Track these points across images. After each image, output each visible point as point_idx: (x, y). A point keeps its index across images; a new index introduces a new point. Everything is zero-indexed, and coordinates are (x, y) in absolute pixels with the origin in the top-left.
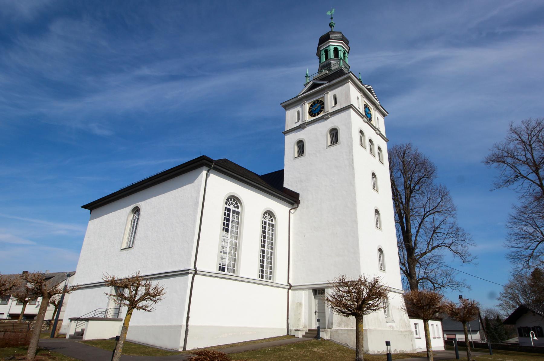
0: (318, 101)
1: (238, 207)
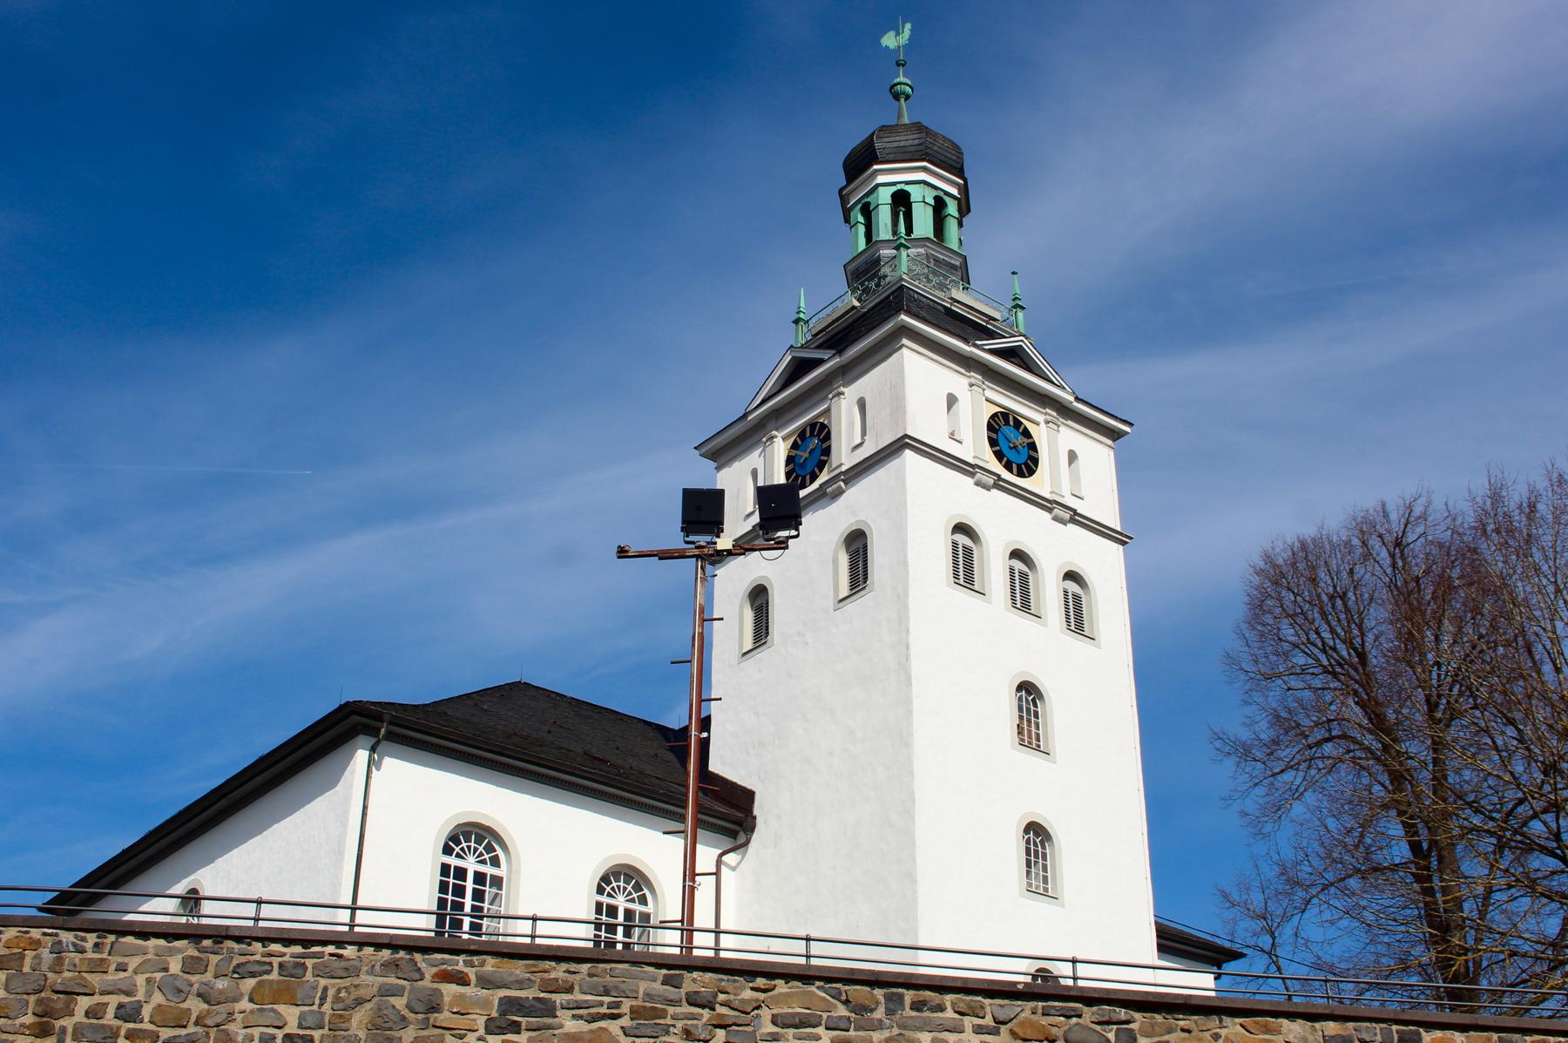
0: (812, 425)
1: (495, 862)
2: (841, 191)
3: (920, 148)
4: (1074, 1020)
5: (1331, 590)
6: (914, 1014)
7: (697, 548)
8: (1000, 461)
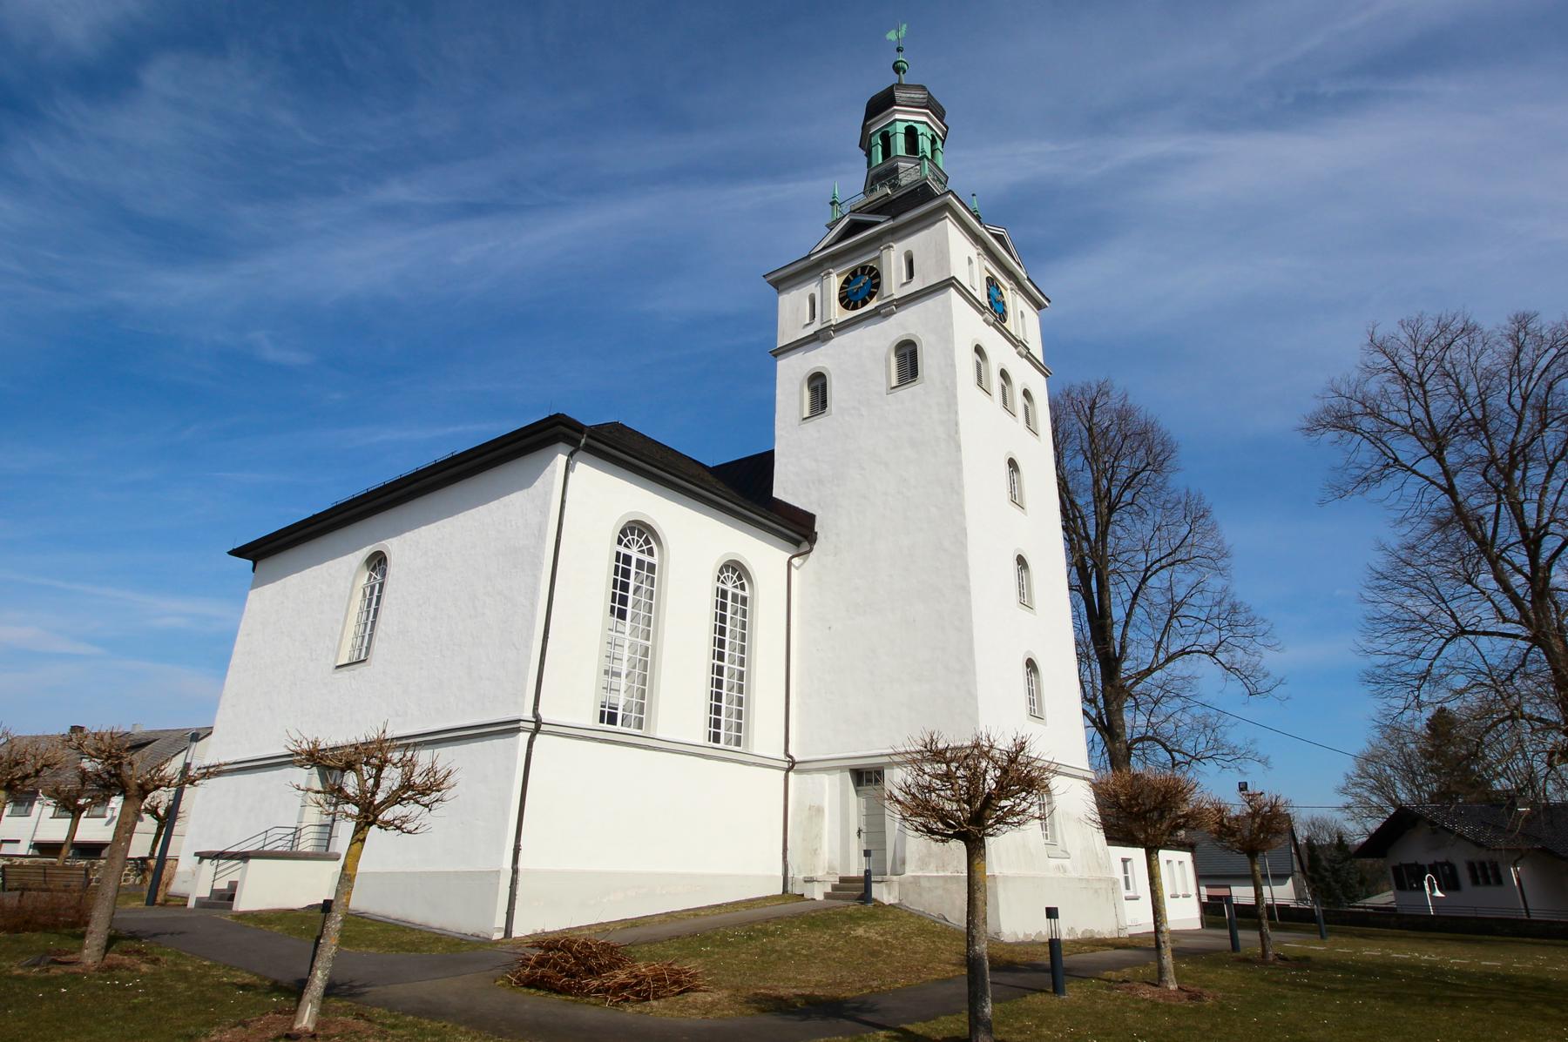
0: (863, 268)
1: (651, 552)
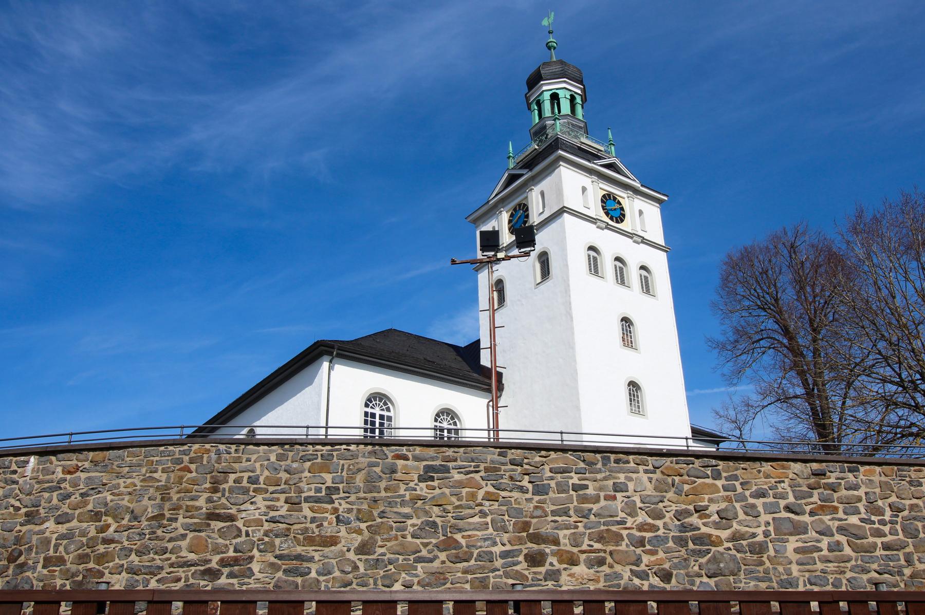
0: (520, 205)
1: (388, 410)
2: (526, 95)
3: (562, 72)
4: (691, 466)
5: (761, 270)
6: (616, 465)
7: (488, 258)
8: (608, 217)
